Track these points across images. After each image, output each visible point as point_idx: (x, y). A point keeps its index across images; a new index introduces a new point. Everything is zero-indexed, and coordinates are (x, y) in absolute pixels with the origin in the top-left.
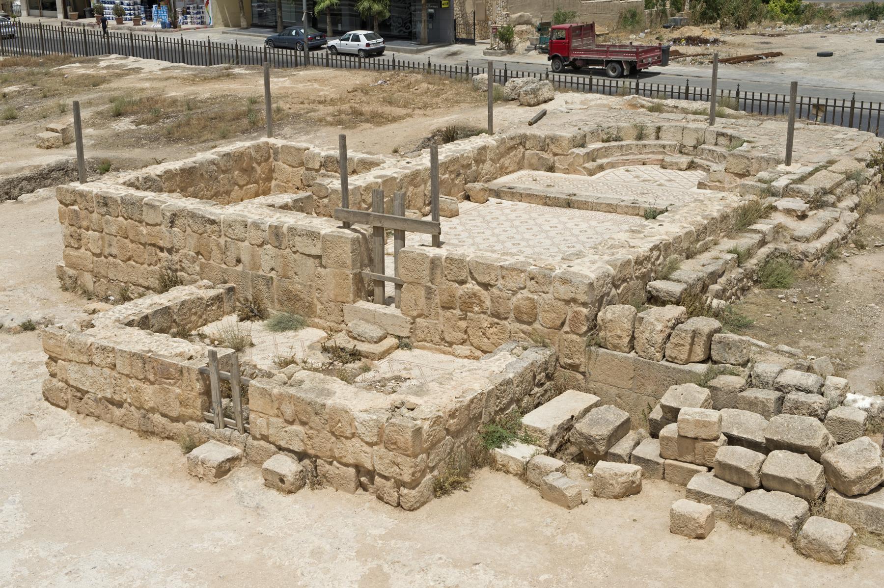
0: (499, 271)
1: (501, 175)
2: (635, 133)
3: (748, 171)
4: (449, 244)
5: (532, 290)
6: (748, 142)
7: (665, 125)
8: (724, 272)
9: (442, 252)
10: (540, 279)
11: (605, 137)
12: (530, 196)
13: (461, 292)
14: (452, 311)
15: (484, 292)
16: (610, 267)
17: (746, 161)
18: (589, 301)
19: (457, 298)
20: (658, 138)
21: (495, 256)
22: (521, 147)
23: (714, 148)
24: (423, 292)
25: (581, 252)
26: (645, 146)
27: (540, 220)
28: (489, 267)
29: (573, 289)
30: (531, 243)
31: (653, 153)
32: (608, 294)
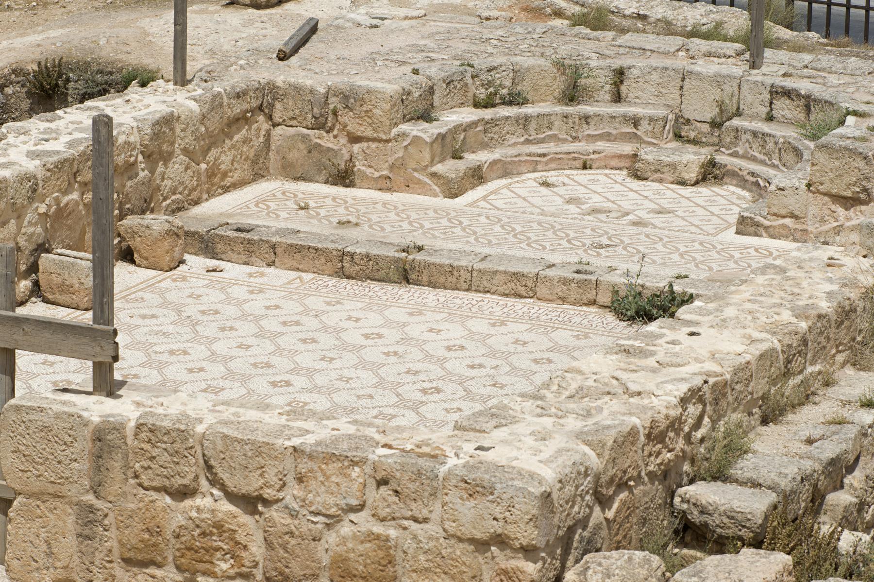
0: (289, 463)
1: (211, 195)
2: (559, 85)
3: (865, 190)
4: (136, 388)
5: (383, 513)
6: (855, 113)
7: (637, 64)
8: (857, 459)
9: (124, 409)
10: (404, 483)
11: (482, 94)
12: (296, 249)
13: (180, 520)
14: (152, 570)
15: (245, 519)
16: (587, 449)
17: (861, 164)
18: (541, 542)
19: (168, 535)
20: (618, 98)
21: (272, 419)
22: (261, 118)
23: (766, 128)
24: (71, 520)
25: (505, 407)
26: (586, 119)
27: (333, 318)
28: (261, 450)
29: (497, 511)
30: (319, 379)
31: (607, 137)
32: (583, 523)
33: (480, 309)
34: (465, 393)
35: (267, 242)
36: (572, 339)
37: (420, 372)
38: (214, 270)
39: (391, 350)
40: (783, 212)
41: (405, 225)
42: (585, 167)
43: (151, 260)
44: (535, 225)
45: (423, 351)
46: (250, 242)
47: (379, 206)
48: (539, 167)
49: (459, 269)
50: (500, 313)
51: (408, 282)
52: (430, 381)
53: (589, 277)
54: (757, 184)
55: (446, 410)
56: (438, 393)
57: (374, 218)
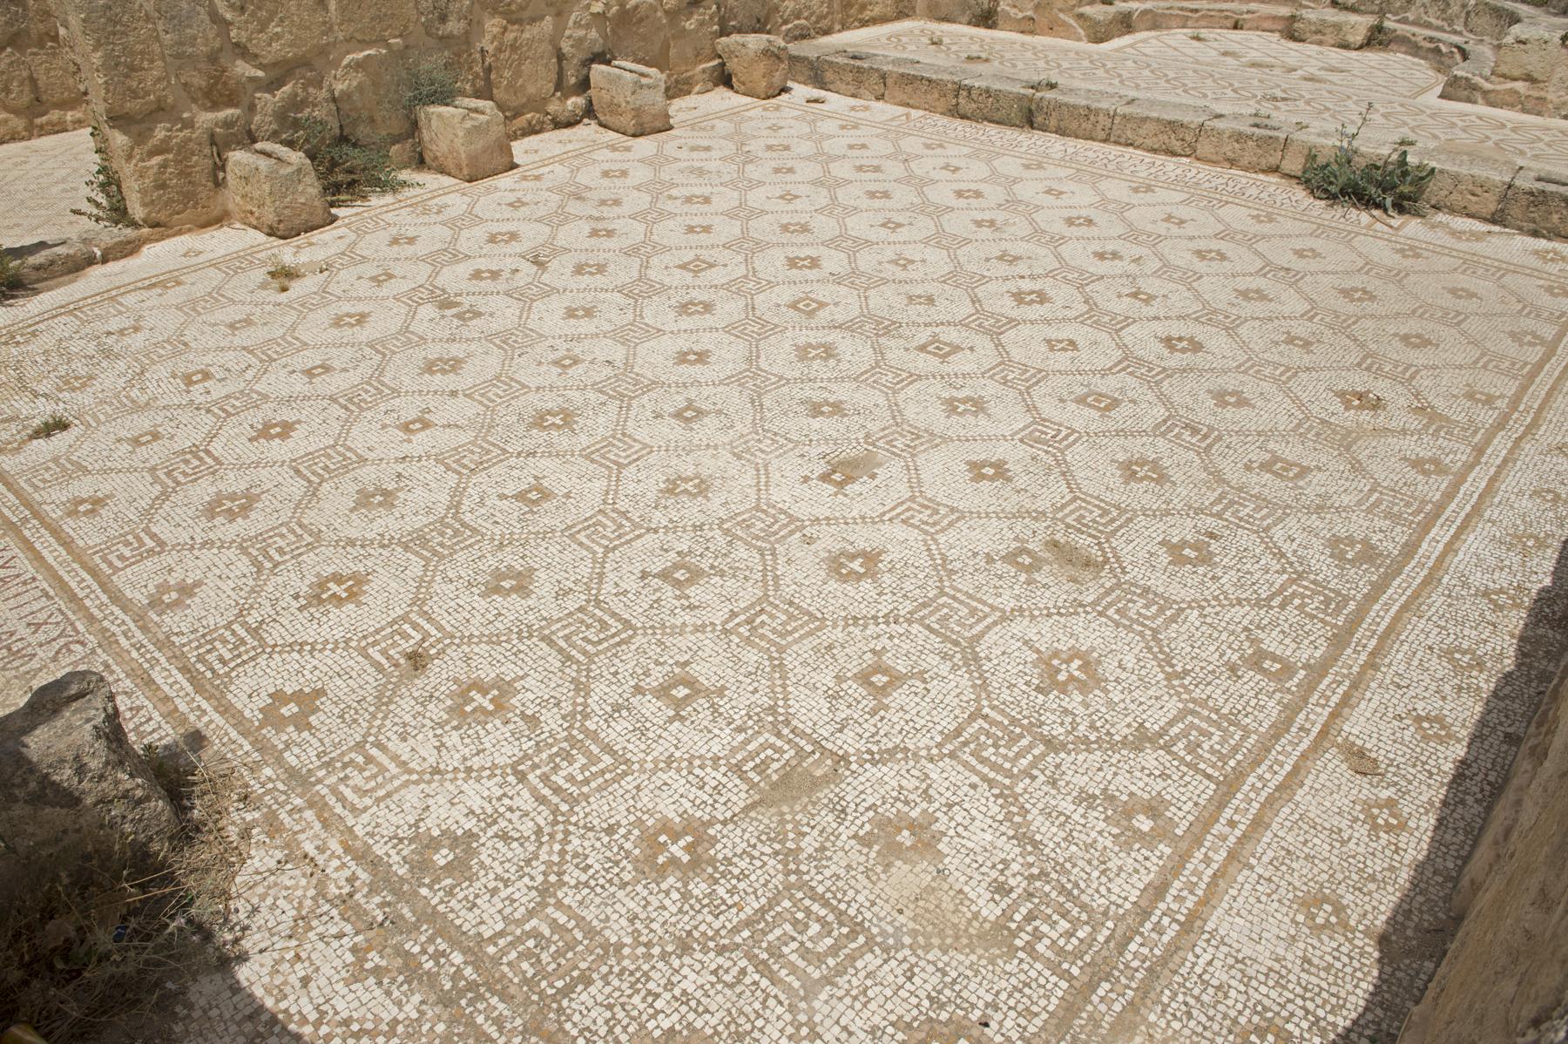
1: (845, 27)
12: (908, 80)
33: (1119, 168)
34: (1085, 308)
35: (877, 70)
36: (1250, 221)
37: (1020, 258)
38: (816, 101)
39: (987, 218)
40: (1516, 73)
41: (1041, 64)
42: (1235, 27)
43: (749, 85)
44: (1190, 73)
45: (1032, 222)
46: (859, 70)
47: (1017, 46)
48: (1190, 23)
49: (1097, 112)
50: (1144, 174)
51: (1032, 127)
52: (1032, 277)
53: (1275, 133)
54: (1437, 51)
55: (1049, 341)
56: (1041, 303)
57: (1008, 55)
